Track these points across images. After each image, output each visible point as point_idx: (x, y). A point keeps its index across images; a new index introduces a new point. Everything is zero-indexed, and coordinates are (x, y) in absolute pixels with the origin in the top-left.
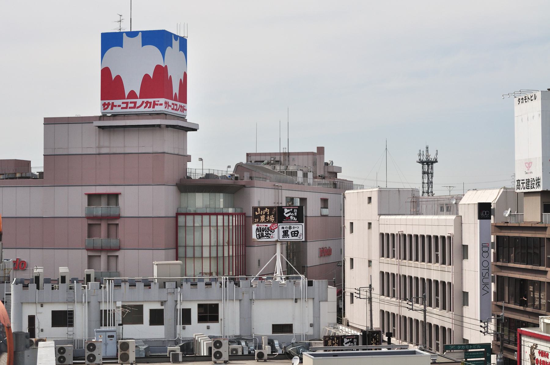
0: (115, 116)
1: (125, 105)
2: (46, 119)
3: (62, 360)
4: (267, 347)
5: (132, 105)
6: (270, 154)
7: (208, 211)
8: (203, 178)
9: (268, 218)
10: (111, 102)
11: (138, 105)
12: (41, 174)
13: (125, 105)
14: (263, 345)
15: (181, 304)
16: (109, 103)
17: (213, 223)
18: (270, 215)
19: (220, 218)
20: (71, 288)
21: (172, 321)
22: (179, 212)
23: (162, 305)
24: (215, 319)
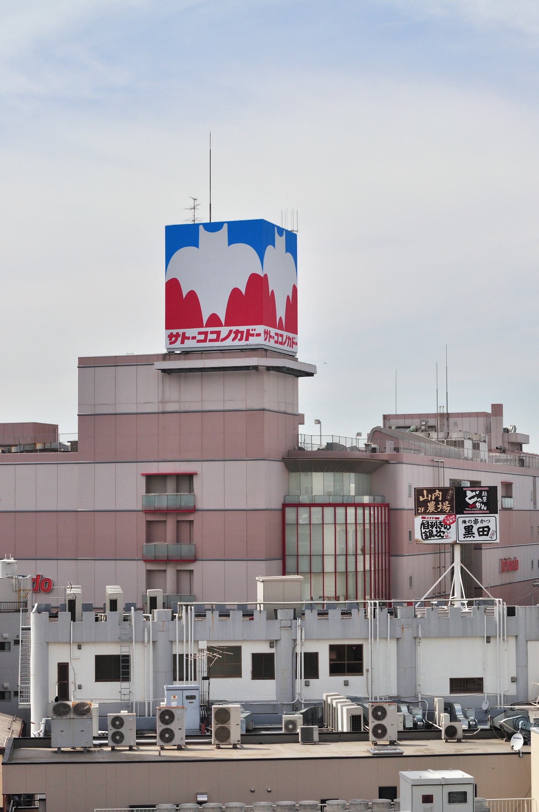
0: (187, 354)
1: (202, 337)
2: (81, 360)
3: (118, 738)
4: (443, 715)
5: (214, 336)
6: (419, 416)
7: (332, 500)
8: (323, 449)
9: (440, 506)
10: (181, 331)
11: (222, 336)
12: (74, 444)
13: (202, 337)
14: (437, 713)
15: (302, 645)
16: (178, 333)
17: (340, 519)
18: (444, 500)
19: (351, 511)
20: (126, 619)
21: (289, 673)
22: (287, 502)
23: (271, 647)
24: (356, 668)
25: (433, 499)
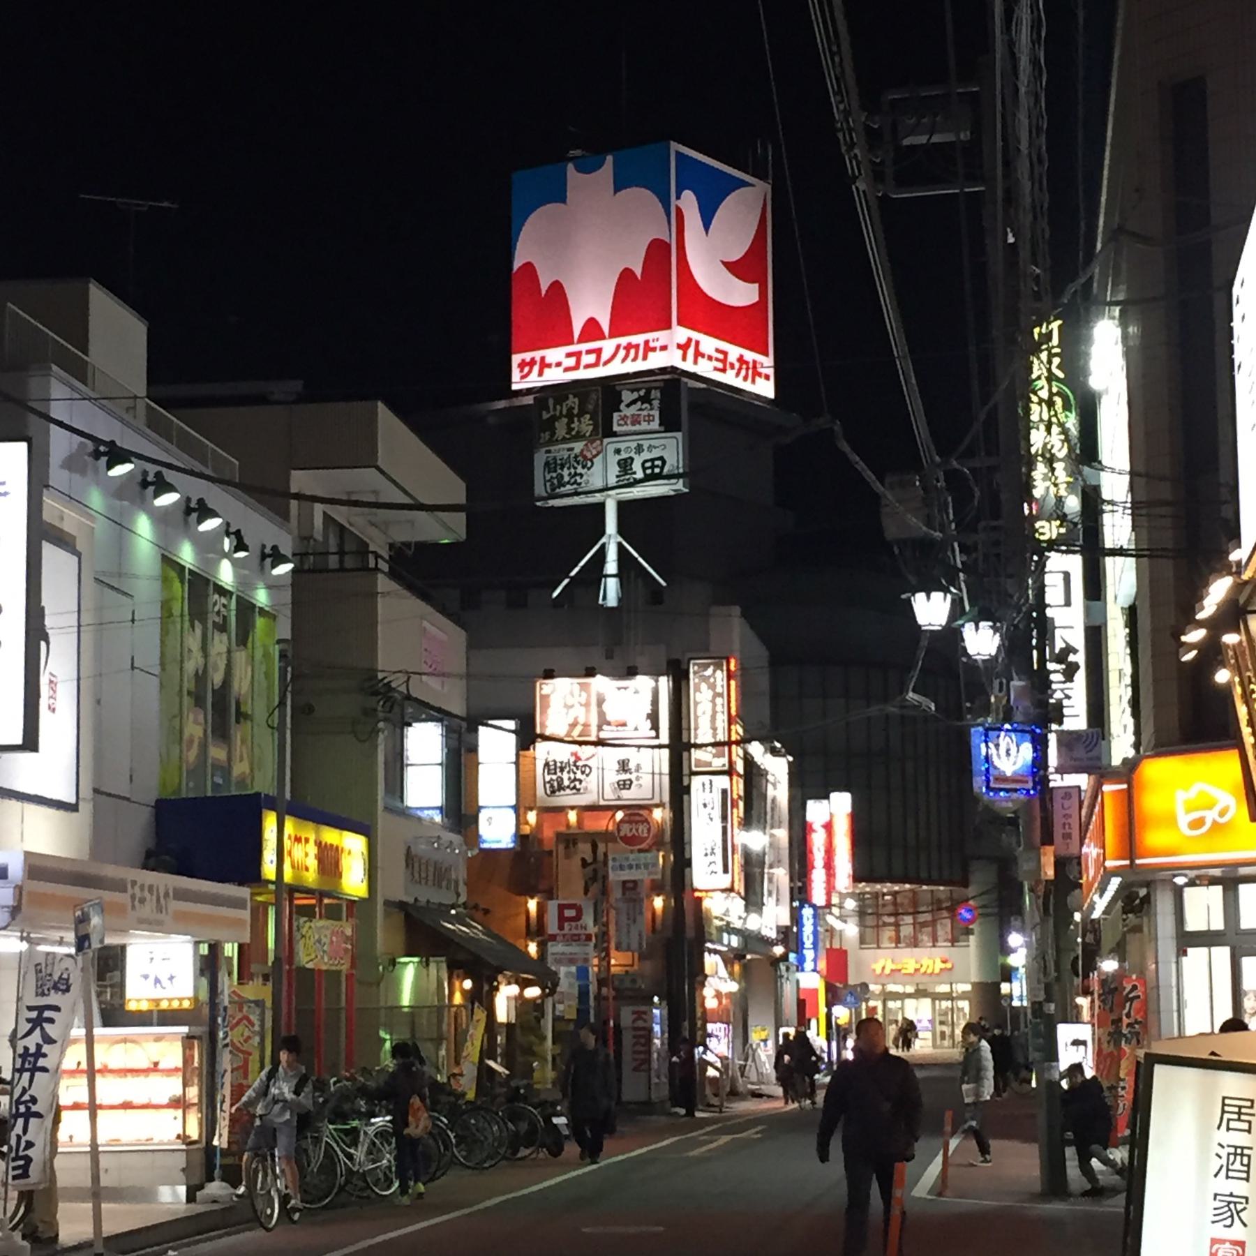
5: (591, 358)
10: (537, 355)
11: (605, 356)
25: (564, 412)
